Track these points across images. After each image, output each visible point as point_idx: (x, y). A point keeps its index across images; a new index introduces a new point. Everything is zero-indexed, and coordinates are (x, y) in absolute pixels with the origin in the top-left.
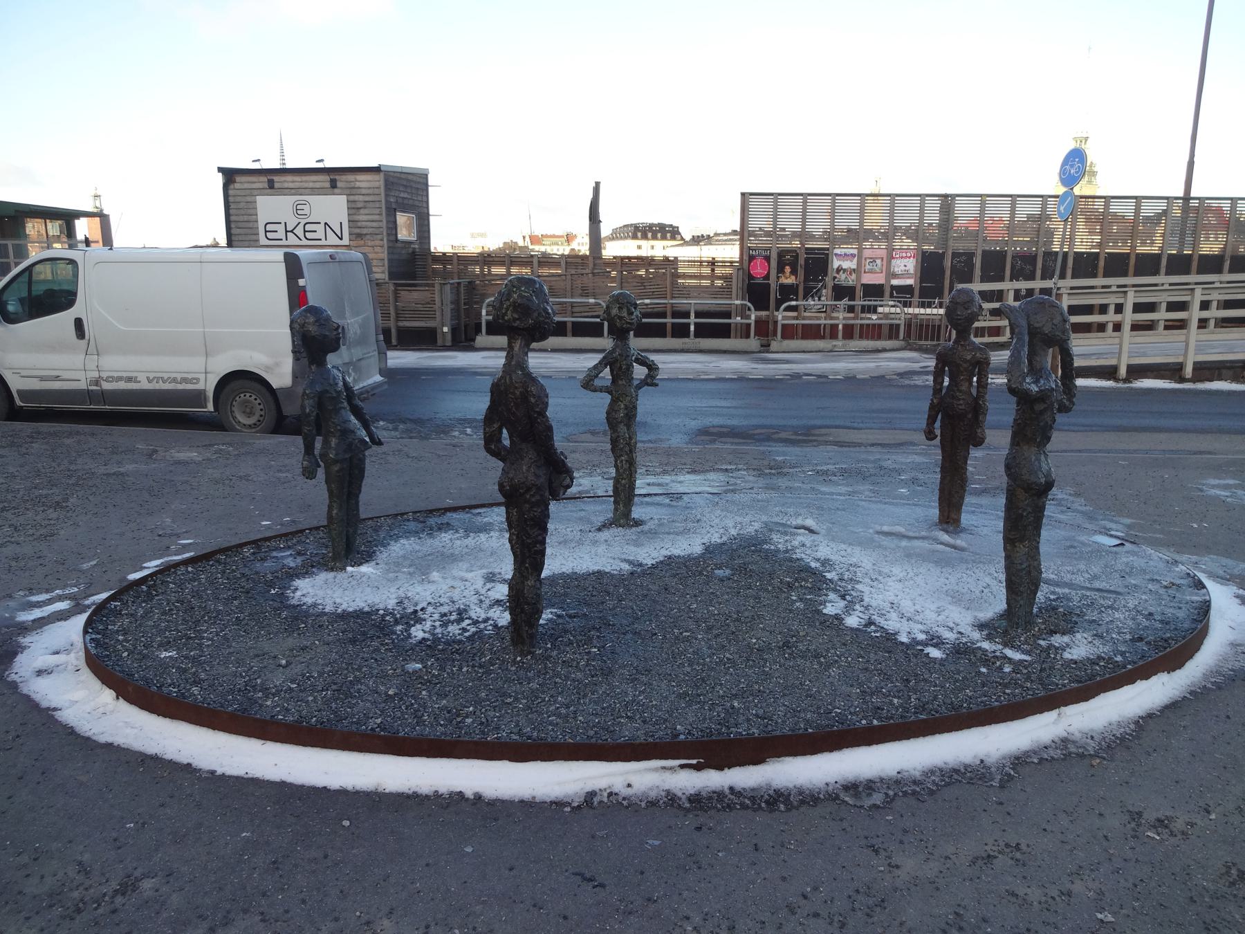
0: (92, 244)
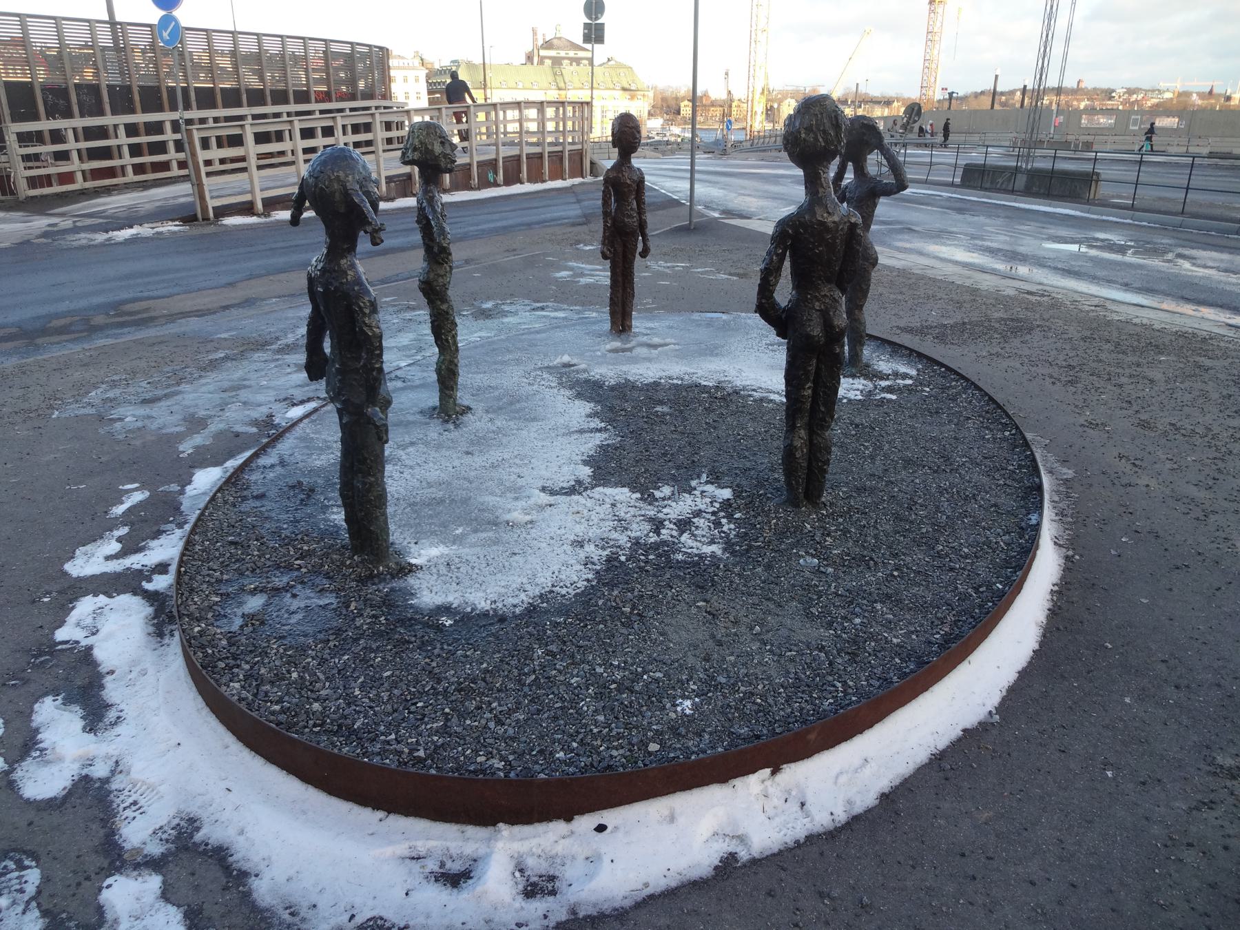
0: (585, 472)
